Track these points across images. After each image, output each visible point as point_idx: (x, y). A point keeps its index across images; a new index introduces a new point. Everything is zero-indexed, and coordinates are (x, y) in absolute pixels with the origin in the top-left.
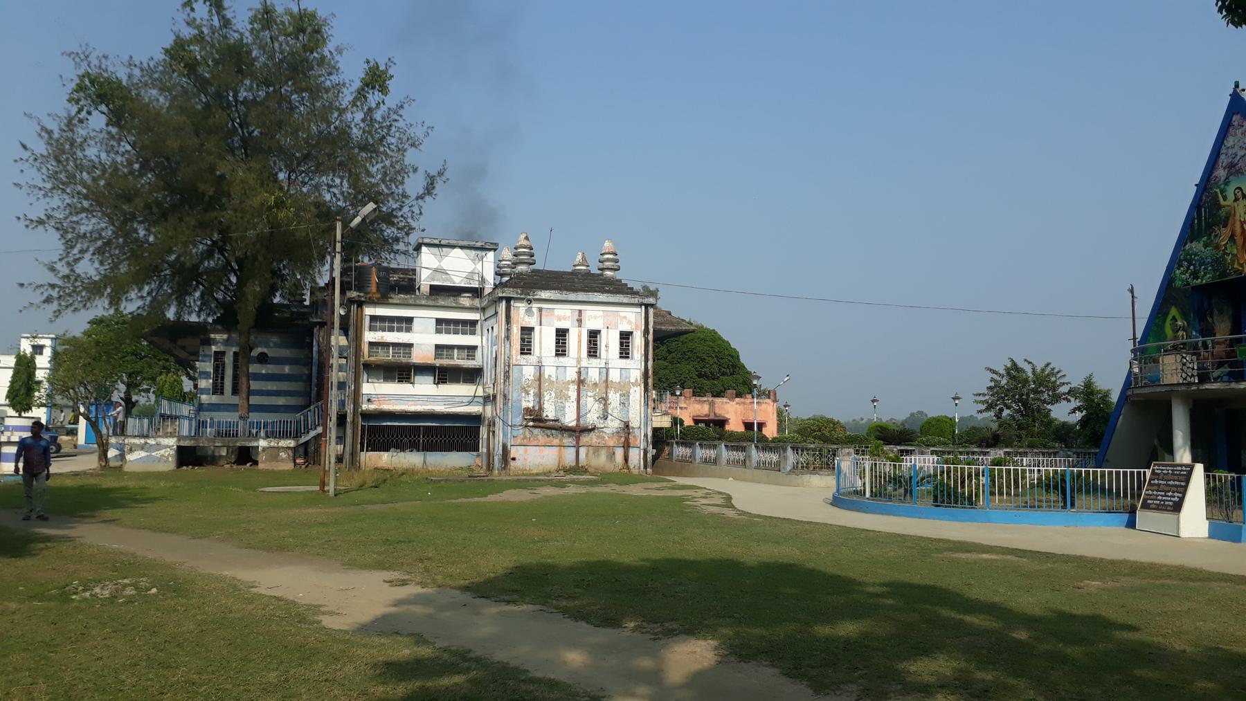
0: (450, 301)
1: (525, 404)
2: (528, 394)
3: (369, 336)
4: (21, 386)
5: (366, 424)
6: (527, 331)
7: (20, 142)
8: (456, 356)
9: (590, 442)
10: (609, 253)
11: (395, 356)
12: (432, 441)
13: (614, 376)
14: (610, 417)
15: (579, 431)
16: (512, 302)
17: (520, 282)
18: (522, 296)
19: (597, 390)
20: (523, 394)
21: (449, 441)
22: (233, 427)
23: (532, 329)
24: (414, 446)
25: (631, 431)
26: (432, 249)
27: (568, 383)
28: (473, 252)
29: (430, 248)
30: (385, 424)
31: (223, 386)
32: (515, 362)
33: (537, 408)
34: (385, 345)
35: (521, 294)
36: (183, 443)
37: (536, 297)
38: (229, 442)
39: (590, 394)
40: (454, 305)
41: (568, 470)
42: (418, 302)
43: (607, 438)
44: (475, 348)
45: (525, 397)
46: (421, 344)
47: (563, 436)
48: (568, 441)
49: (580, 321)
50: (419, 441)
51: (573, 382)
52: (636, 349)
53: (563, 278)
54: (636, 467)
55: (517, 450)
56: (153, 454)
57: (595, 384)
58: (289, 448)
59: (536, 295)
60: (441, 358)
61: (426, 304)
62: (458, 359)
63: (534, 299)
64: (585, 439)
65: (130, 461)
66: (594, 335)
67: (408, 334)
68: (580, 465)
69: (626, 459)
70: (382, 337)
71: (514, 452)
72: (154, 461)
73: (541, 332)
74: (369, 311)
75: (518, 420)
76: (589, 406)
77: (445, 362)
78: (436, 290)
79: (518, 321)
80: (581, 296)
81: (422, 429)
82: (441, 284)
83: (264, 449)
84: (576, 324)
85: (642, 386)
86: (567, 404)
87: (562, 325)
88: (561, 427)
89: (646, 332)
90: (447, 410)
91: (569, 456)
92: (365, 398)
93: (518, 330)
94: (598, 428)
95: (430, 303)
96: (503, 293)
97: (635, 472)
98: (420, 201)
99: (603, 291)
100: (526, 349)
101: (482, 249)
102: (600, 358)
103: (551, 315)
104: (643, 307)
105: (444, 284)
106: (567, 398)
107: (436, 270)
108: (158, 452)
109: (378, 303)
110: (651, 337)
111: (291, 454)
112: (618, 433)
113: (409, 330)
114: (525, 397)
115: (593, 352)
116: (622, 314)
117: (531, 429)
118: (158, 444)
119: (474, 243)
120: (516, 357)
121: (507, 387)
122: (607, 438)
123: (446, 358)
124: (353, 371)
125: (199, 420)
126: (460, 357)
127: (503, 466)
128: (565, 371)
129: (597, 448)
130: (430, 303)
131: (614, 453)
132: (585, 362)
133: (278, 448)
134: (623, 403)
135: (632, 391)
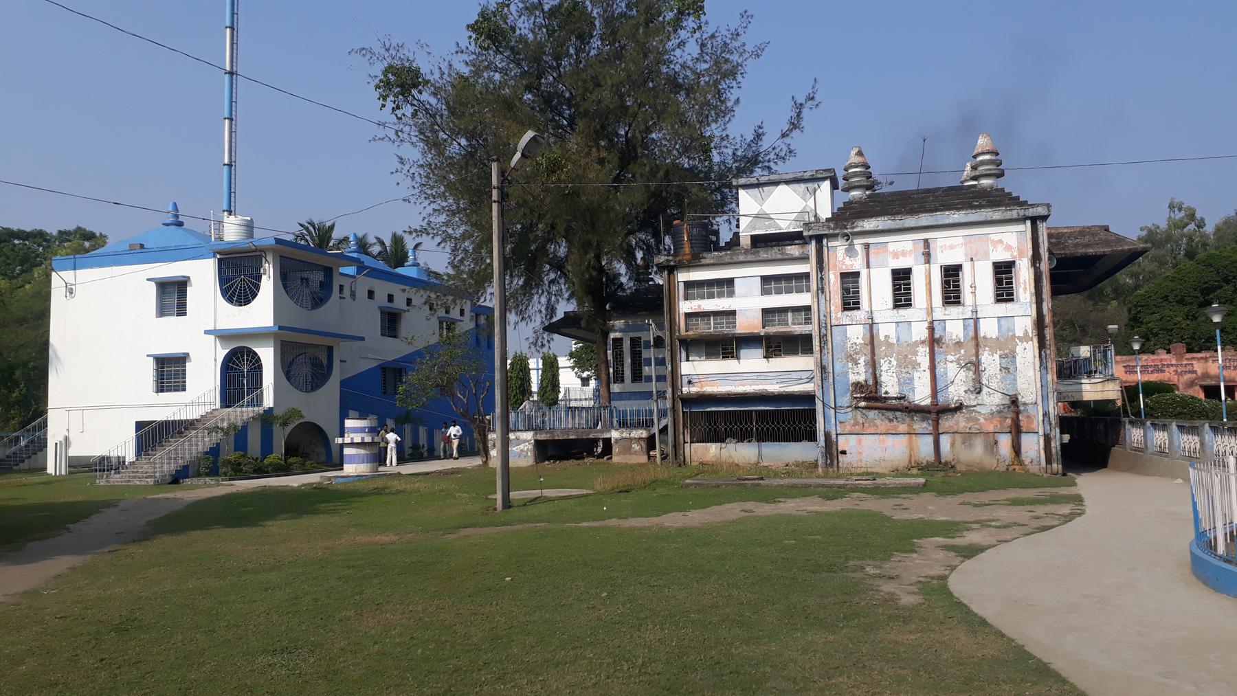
0: (774, 253)
1: (853, 378)
2: (857, 364)
3: (685, 307)
4: (548, 384)
6: (850, 278)
7: (397, 156)
8: (790, 321)
9: (955, 427)
10: (983, 153)
11: (717, 328)
12: (768, 429)
13: (989, 329)
14: (985, 390)
15: (937, 412)
16: (825, 241)
17: (845, 213)
18: (837, 231)
19: (962, 351)
23: (856, 275)
24: (744, 437)
25: (1022, 408)
26: (750, 191)
27: (916, 344)
28: (802, 186)
29: (748, 191)
30: (709, 409)
31: (623, 377)
32: (834, 322)
33: (871, 382)
34: (705, 315)
35: (834, 229)
36: (542, 437)
37: (855, 230)
39: (950, 358)
40: (779, 256)
41: (924, 468)
42: (735, 259)
43: (982, 420)
44: (807, 309)
45: (853, 369)
46: (745, 310)
47: (912, 419)
48: (921, 426)
49: (928, 257)
50: (752, 429)
51: (923, 342)
52: (1023, 286)
53: (911, 199)
54: (1035, 462)
55: (847, 441)
56: (514, 449)
57: (959, 344)
58: (640, 439)
59: (857, 226)
60: (773, 325)
61: (745, 260)
62: (793, 324)
63: (851, 233)
64: (947, 423)
66: (952, 274)
68: (943, 461)
69: (1017, 448)
70: (699, 306)
71: (843, 443)
72: (515, 456)
73: (869, 276)
74: (683, 276)
75: (845, 400)
76: (951, 375)
77: (772, 330)
78: (760, 241)
79: (835, 266)
80: (924, 219)
81: (754, 414)
82: (764, 233)
83: (617, 441)
84: (922, 259)
85: (1035, 340)
86: (916, 375)
87: (901, 264)
88: (907, 408)
89: (1036, 258)
90: (782, 390)
91: (924, 448)
92: (685, 380)
94: (967, 406)
95: (750, 258)
97: (1034, 469)
98: (787, 140)
99: (957, 208)
100: (850, 302)
101: (813, 179)
102: (963, 305)
103: (884, 251)
104: (1029, 223)
106: (916, 365)
107: (757, 217)
108: (518, 447)
110: (1045, 266)
111: (644, 445)
112: (1000, 412)
113: (731, 294)
114: (853, 369)
115: (952, 294)
116: (995, 237)
117: (864, 411)
118: (517, 439)
121: (825, 357)
122: (982, 420)
124: (669, 348)
127: (829, 461)
128: (910, 329)
129: (968, 436)
130: (750, 258)
131: (996, 443)
132: (940, 312)
133: (631, 439)
134: (1007, 368)
135: (1019, 349)
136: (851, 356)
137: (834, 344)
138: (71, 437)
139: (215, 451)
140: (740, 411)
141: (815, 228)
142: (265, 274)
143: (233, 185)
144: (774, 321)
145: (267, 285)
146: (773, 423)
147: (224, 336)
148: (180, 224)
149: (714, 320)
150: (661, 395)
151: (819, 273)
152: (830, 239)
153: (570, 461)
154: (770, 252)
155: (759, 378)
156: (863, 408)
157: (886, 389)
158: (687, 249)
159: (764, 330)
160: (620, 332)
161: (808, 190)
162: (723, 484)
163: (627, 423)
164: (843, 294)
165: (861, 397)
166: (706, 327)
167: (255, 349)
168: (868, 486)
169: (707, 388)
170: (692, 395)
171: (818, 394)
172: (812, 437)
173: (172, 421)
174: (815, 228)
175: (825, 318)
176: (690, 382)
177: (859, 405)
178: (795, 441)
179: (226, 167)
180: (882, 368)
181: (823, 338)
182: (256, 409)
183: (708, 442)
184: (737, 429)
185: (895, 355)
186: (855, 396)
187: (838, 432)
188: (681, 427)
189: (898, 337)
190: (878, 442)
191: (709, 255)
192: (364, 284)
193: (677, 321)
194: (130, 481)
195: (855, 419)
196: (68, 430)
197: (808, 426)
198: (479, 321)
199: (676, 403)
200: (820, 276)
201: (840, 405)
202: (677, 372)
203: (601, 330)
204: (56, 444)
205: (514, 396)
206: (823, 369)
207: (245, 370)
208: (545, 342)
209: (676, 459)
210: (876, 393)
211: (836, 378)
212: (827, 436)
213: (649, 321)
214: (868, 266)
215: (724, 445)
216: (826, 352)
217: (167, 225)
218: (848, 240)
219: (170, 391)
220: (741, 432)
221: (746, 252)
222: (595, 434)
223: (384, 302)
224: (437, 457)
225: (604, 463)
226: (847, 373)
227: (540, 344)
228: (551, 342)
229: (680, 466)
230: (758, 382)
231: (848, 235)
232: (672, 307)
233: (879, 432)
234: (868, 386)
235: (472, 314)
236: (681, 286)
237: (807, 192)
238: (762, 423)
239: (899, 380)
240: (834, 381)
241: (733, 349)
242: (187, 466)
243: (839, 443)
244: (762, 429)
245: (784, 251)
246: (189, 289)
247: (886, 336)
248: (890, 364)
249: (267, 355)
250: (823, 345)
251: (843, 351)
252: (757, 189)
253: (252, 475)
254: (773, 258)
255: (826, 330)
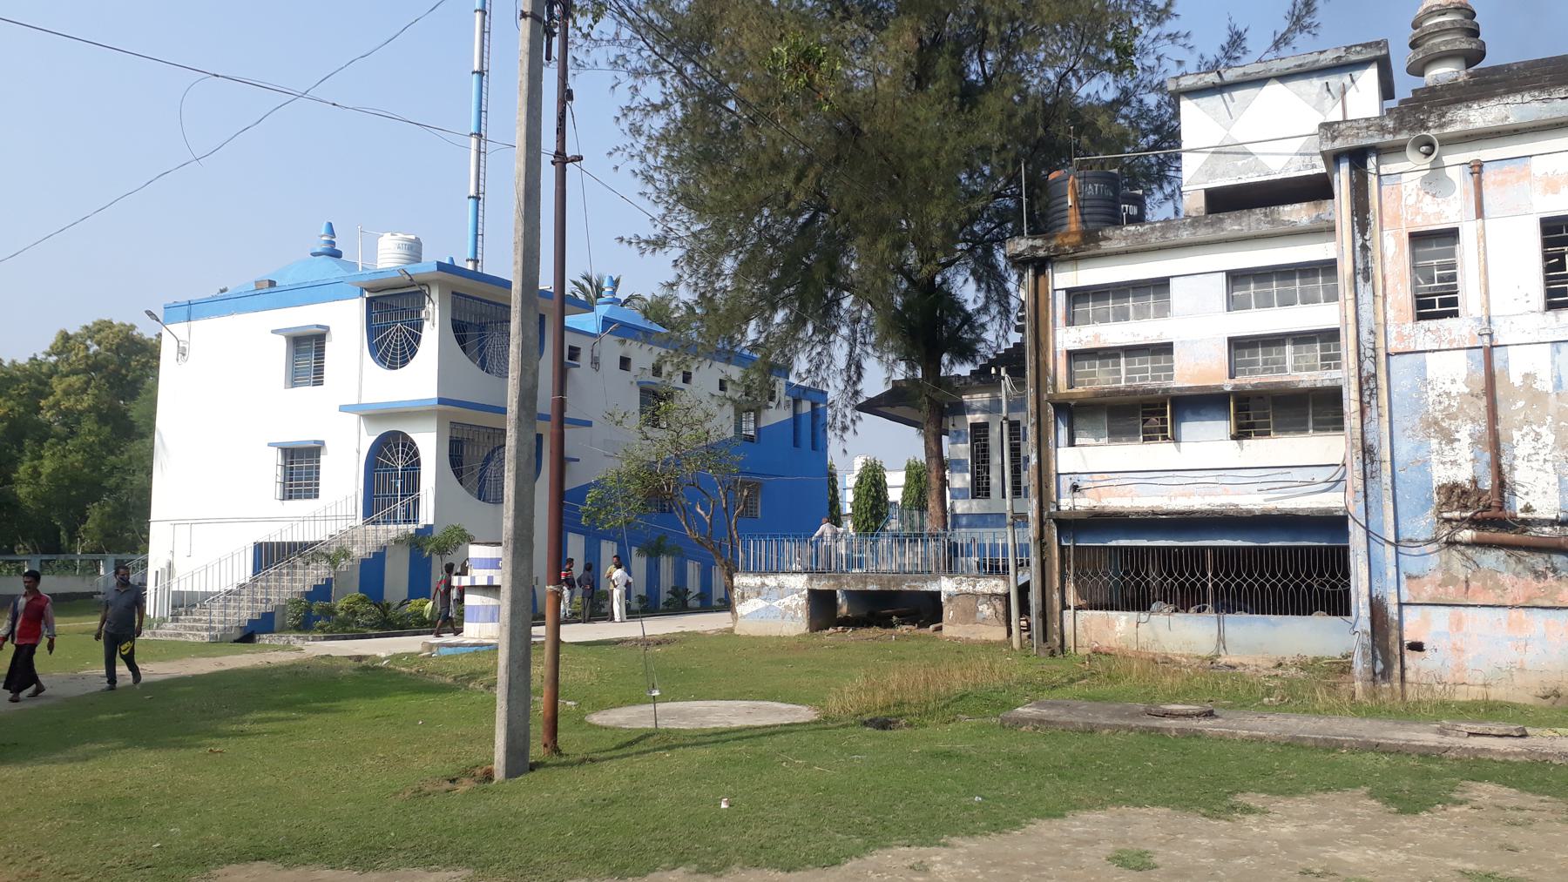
0: (1254, 221)
1: (1441, 474)
2: (1451, 441)
5: (1070, 544)
11: (1134, 379)
16: (1371, 163)
20: (1434, 443)
21: (1285, 586)
22: (817, 565)
23: (1451, 235)
24: (1187, 599)
28: (1317, 83)
29: (1200, 101)
31: (988, 489)
32: (1394, 346)
33: (1487, 484)
35: (1396, 131)
37: (1449, 130)
38: (889, 581)
40: (1265, 228)
44: (1331, 336)
45: (1441, 453)
50: (1204, 586)
60: (1252, 372)
61: (1192, 238)
62: (1297, 369)
65: (743, 616)
67: (1161, 322)
70: (1096, 337)
71: (1414, 624)
72: (775, 617)
73: (1482, 237)
74: (1064, 278)
75: (1421, 525)
77: (1247, 380)
78: (1223, 201)
79: (1397, 218)
83: (950, 597)
92: (1066, 483)
93: (1399, 244)
95: (1203, 234)
96: (1334, 139)
105: (1240, 182)
107: (1219, 151)
108: (782, 601)
109: (1076, 259)
113: (1164, 311)
114: (1441, 453)
117: (1469, 552)
118: (780, 587)
119: (1315, 57)
120: (1402, 327)
121: (1373, 425)
123: (1265, 371)
125: (956, 544)
126: (1303, 364)
127: (1380, 666)
133: (976, 595)
136: (1436, 423)
137: (1394, 396)
138: (176, 565)
139: (322, 592)
140: (1180, 548)
141: (1347, 132)
142: (428, 319)
143: (480, 226)
144: (1254, 363)
145: (431, 336)
146: (1250, 575)
147: (372, 415)
148: (336, 254)
149: (1127, 364)
150: (1020, 520)
151: (1358, 236)
152: (1384, 158)
153: (871, 630)
154: (1245, 219)
155: (1221, 480)
156: (1468, 545)
157: (1528, 499)
158: (1073, 223)
159: (1233, 382)
160: (983, 411)
161: (1329, 90)
162: (1105, 726)
163: (998, 567)
164: (1417, 283)
165: (1463, 519)
166: (1111, 378)
167: (411, 435)
168: (1511, 758)
169: (1109, 499)
170: (1079, 512)
171: (1357, 510)
172: (1338, 604)
173: (289, 543)
174: (1347, 132)
175: (1371, 337)
176: (1075, 488)
177: (1458, 538)
178: (1299, 614)
179: (471, 200)
180: (1516, 452)
181: (1367, 384)
182: (403, 527)
183: (1112, 610)
184: (1173, 584)
185: (1549, 419)
186: (1446, 515)
187: (1404, 600)
188: (1056, 577)
189: (1560, 380)
190: (1505, 625)
191: (1118, 232)
192: (612, 350)
193: (1051, 366)
194: (180, 635)
195: (1447, 570)
196: (172, 552)
197: (1328, 582)
198: (799, 409)
199: (1046, 528)
200: (1359, 242)
201: (1409, 536)
202: (1048, 468)
203: (929, 398)
204: (157, 572)
205: (864, 522)
206: (1367, 452)
207: (400, 467)
208: (848, 422)
209: (1045, 640)
210: (1501, 509)
211: (1400, 474)
212: (1377, 608)
213: (998, 371)
214: (1480, 213)
215: (1143, 616)
216: (1374, 414)
217: (314, 254)
218: (1428, 155)
219: (299, 497)
220: (1182, 592)
221: (1196, 222)
222: (914, 584)
223: (649, 377)
224: (606, 614)
225: (926, 637)
226: (1426, 463)
227: (839, 424)
228: (858, 423)
229: (1052, 654)
230: (1220, 489)
231: (1431, 145)
232: (1042, 338)
233: (1509, 603)
234: (1480, 493)
235: (788, 398)
236: (1061, 298)
237: (1326, 94)
238: (1227, 575)
239: (1560, 479)
240: (1393, 482)
241: (1164, 421)
242: (272, 614)
243: (1406, 625)
244: (1227, 586)
245: (1276, 216)
246: (327, 345)
247: (1526, 376)
248: (1536, 440)
249: (427, 443)
250: (1366, 399)
251: (1416, 412)
252: (1219, 96)
253: (370, 632)
254: (1254, 232)
255: (1375, 364)
